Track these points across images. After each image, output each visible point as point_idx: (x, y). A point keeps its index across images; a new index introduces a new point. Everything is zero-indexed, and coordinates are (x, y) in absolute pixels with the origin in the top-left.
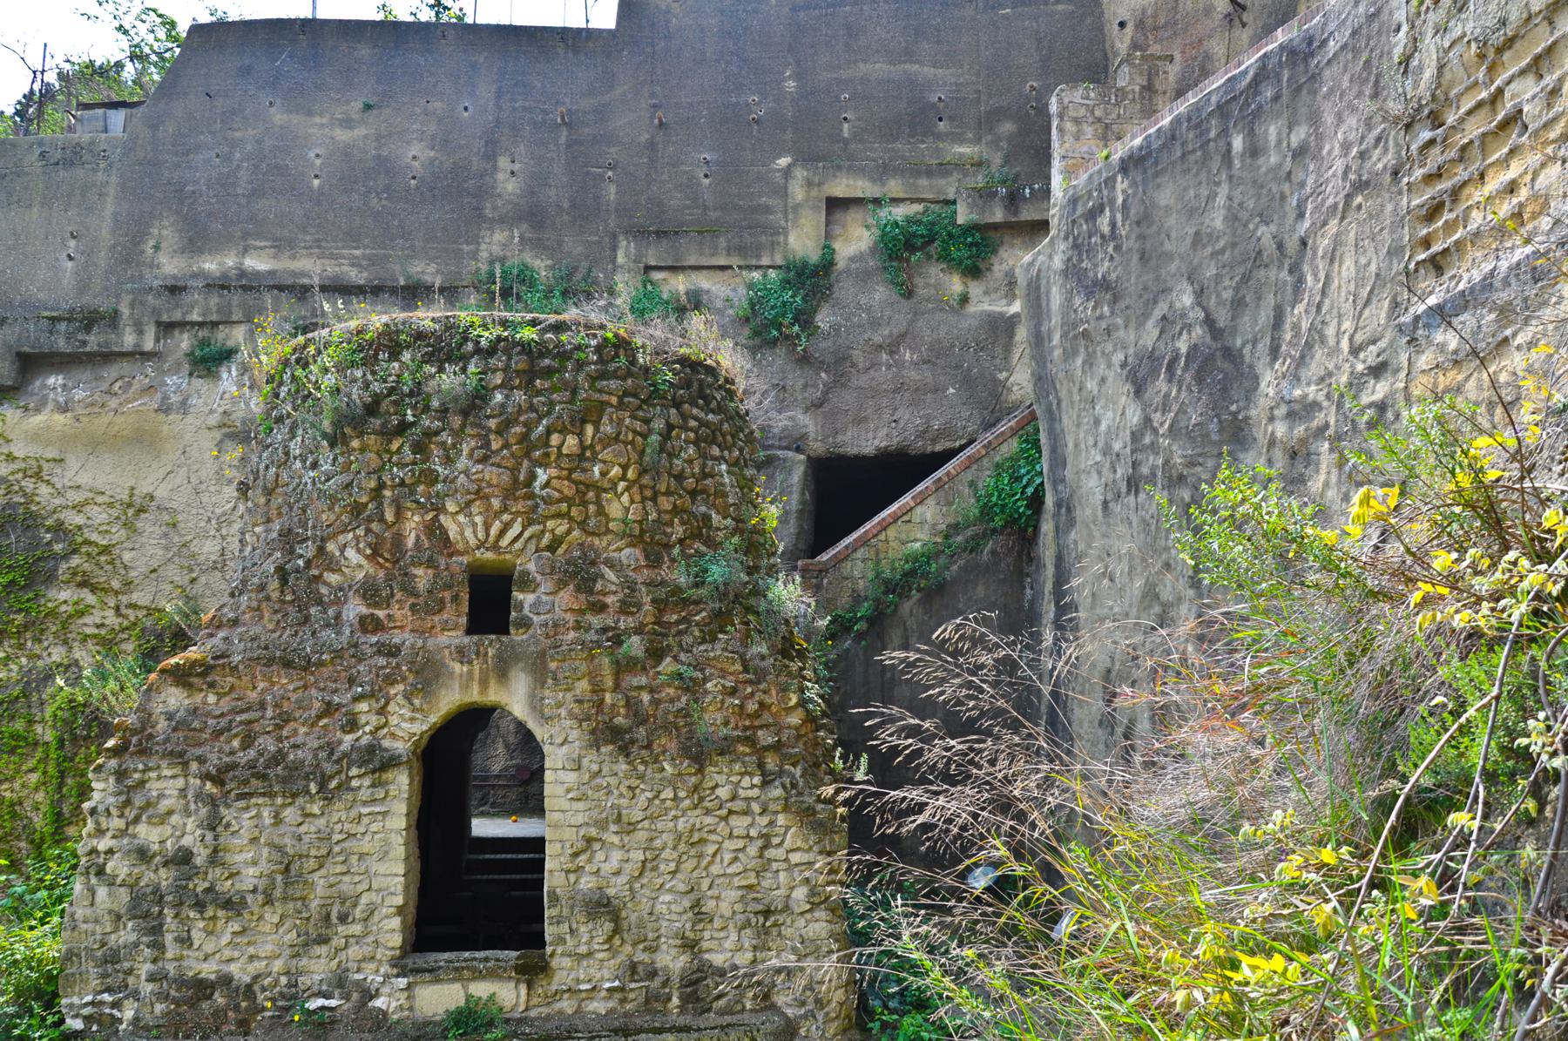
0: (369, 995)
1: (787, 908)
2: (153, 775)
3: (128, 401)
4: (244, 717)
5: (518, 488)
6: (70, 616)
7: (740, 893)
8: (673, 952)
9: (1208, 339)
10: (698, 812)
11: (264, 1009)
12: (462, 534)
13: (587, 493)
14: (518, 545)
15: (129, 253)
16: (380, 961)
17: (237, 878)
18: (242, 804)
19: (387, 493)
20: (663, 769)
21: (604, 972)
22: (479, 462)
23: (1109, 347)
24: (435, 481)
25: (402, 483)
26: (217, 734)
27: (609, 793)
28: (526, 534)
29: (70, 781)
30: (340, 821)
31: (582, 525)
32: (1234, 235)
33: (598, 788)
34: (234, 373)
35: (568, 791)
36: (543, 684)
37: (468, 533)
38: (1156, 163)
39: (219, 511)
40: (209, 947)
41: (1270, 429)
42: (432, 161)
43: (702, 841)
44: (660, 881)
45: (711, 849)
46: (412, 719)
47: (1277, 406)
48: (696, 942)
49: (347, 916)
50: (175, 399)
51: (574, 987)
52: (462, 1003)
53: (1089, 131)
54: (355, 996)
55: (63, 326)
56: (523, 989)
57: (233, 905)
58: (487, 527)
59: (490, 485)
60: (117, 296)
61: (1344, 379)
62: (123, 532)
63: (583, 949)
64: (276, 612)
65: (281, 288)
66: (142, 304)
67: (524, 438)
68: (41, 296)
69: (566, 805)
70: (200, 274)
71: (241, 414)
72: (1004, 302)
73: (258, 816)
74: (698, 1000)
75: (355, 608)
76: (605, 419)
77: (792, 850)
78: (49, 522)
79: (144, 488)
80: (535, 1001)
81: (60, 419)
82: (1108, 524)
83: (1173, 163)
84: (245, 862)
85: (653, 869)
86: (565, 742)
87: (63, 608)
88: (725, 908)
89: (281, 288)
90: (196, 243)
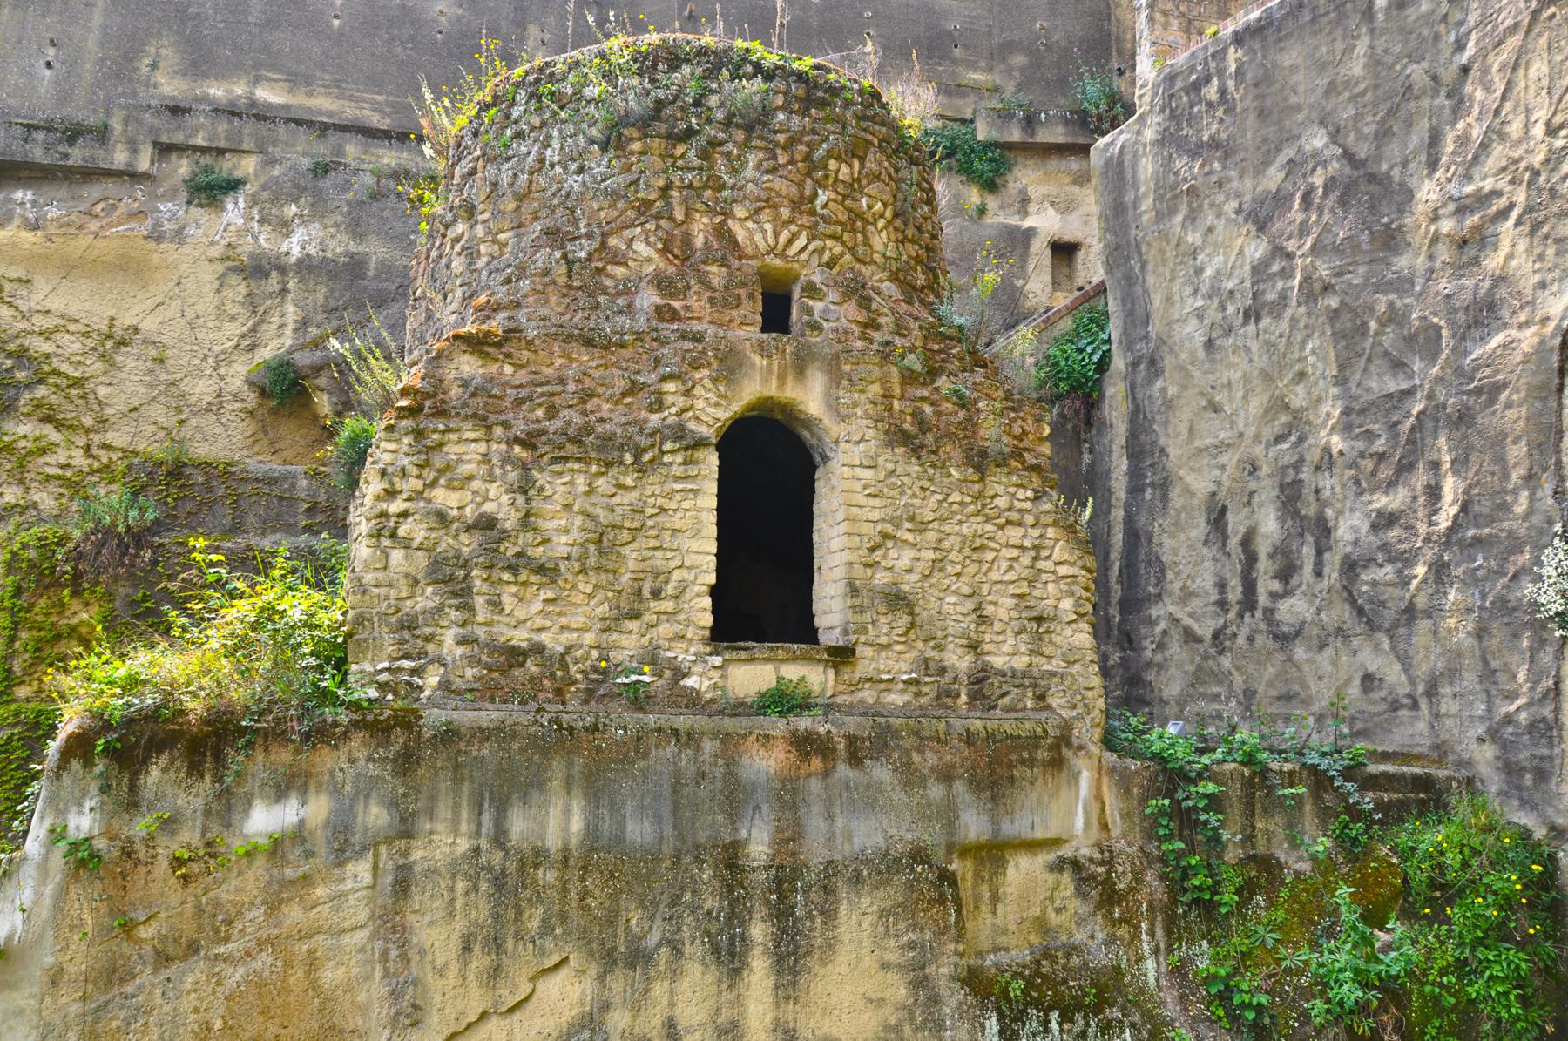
0: (680, 674)
2: (454, 437)
3: (111, 225)
4: (545, 389)
5: (802, 203)
6: (30, 453)
7: (1014, 601)
8: (959, 651)
9: (1347, 171)
10: (979, 519)
11: (575, 682)
12: (751, 239)
13: (857, 221)
14: (804, 256)
15: (121, 67)
17: (548, 545)
18: (556, 468)
19: (675, 193)
20: (950, 475)
21: (900, 665)
22: (767, 172)
23: (1221, 198)
24: (723, 187)
25: (690, 186)
26: (519, 402)
27: (903, 493)
28: (811, 247)
29: (24, 635)
30: (653, 495)
31: (852, 250)
32: (1377, 77)
33: (893, 487)
34: (241, 204)
35: (865, 487)
36: (838, 384)
37: (758, 238)
38: (1279, 30)
39: (217, 349)
40: (521, 613)
41: (1433, 228)
42: (459, 19)
43: (983, 548)
44: (947, 581)
45: (990, 556)
46: (717, 405)
47: (1444, 205)
49: (660, 591)
50: (167, 226)
51: (876, 677)
52: (774, 684)
53: (1175, 24)
54: (668, 674)
55: (40, 136)
57: (547, 571)
58: (776, 235)
59: (779, 196)
60: (107, 112)
61: (1541, 157)
62: (100, 366)
63: (884, 640)
64: (565, 296)
65: (299, 122)
66: (139, 121)
67: (808, 157)
68: (11, 101)
69: (863, 500)
70: (205, 99)
71: (248, 248)
72: (1017, 217)
73: (571, 483)
74: (984, 697)
75: (648, 299)
76: (870, 157)
77: (1060, 563)
78: (10, 347)
79: (127, 319)
80: (841, 688)
81: (28, 236)
82: (1213, 361)
83: (1301, 28)
84: (558, 530)
85: (941, 570)
86: (862, 440)
87: (23, 443)
88: (1002, 613)
89: (299, 122)
90: (199, 64)
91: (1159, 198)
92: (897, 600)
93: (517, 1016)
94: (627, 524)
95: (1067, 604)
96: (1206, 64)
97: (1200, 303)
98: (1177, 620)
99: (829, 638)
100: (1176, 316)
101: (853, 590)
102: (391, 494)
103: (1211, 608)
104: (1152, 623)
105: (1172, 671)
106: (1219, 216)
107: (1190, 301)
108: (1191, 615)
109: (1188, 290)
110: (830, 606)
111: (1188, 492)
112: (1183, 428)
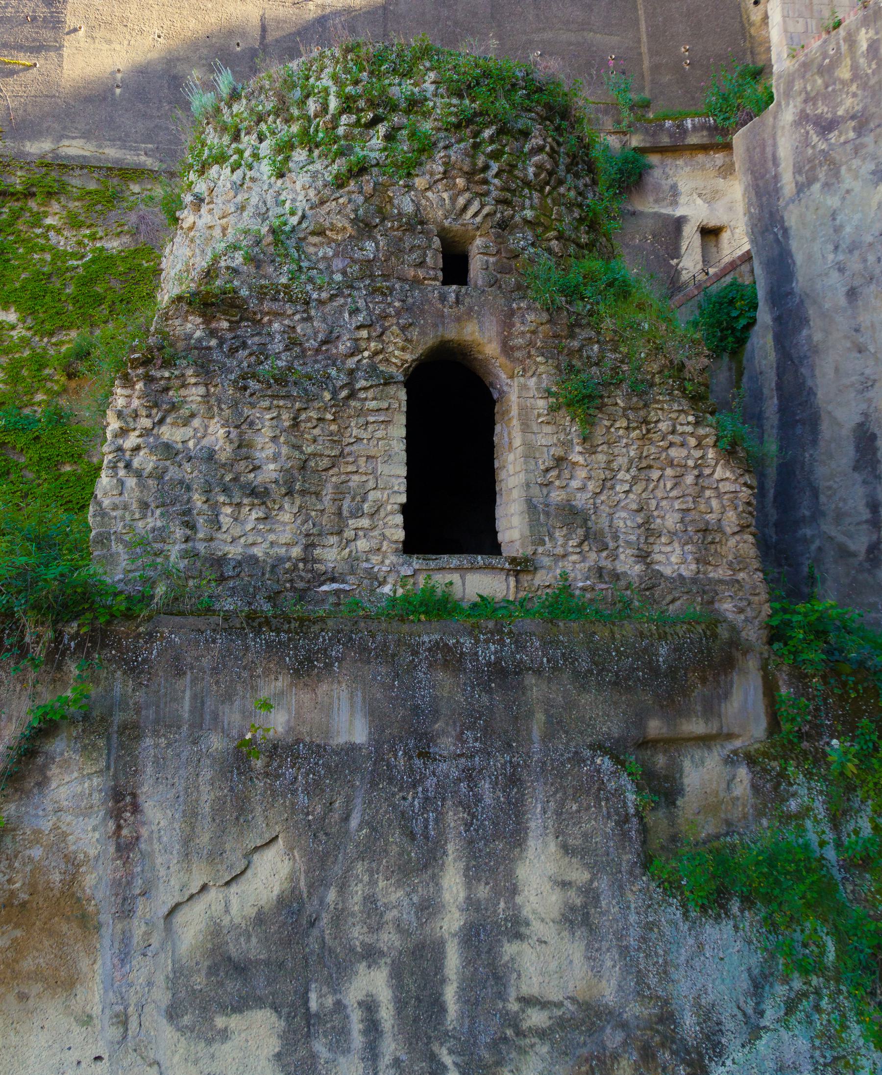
1: (720, 529)
17: (257, 472)
40: (236, 531)
46: (403, 349)
48: (649, 554)
57: (259, 494)
63: (559, 551)
73: (277, 417)
92: (573, 516)
93: (234, 888)
94: (327, 452)
95: (731, 516)
101: (531, 506)
102: (123, 432)
108: (844, 533)
109: (831, 247)
110: (512, 525)
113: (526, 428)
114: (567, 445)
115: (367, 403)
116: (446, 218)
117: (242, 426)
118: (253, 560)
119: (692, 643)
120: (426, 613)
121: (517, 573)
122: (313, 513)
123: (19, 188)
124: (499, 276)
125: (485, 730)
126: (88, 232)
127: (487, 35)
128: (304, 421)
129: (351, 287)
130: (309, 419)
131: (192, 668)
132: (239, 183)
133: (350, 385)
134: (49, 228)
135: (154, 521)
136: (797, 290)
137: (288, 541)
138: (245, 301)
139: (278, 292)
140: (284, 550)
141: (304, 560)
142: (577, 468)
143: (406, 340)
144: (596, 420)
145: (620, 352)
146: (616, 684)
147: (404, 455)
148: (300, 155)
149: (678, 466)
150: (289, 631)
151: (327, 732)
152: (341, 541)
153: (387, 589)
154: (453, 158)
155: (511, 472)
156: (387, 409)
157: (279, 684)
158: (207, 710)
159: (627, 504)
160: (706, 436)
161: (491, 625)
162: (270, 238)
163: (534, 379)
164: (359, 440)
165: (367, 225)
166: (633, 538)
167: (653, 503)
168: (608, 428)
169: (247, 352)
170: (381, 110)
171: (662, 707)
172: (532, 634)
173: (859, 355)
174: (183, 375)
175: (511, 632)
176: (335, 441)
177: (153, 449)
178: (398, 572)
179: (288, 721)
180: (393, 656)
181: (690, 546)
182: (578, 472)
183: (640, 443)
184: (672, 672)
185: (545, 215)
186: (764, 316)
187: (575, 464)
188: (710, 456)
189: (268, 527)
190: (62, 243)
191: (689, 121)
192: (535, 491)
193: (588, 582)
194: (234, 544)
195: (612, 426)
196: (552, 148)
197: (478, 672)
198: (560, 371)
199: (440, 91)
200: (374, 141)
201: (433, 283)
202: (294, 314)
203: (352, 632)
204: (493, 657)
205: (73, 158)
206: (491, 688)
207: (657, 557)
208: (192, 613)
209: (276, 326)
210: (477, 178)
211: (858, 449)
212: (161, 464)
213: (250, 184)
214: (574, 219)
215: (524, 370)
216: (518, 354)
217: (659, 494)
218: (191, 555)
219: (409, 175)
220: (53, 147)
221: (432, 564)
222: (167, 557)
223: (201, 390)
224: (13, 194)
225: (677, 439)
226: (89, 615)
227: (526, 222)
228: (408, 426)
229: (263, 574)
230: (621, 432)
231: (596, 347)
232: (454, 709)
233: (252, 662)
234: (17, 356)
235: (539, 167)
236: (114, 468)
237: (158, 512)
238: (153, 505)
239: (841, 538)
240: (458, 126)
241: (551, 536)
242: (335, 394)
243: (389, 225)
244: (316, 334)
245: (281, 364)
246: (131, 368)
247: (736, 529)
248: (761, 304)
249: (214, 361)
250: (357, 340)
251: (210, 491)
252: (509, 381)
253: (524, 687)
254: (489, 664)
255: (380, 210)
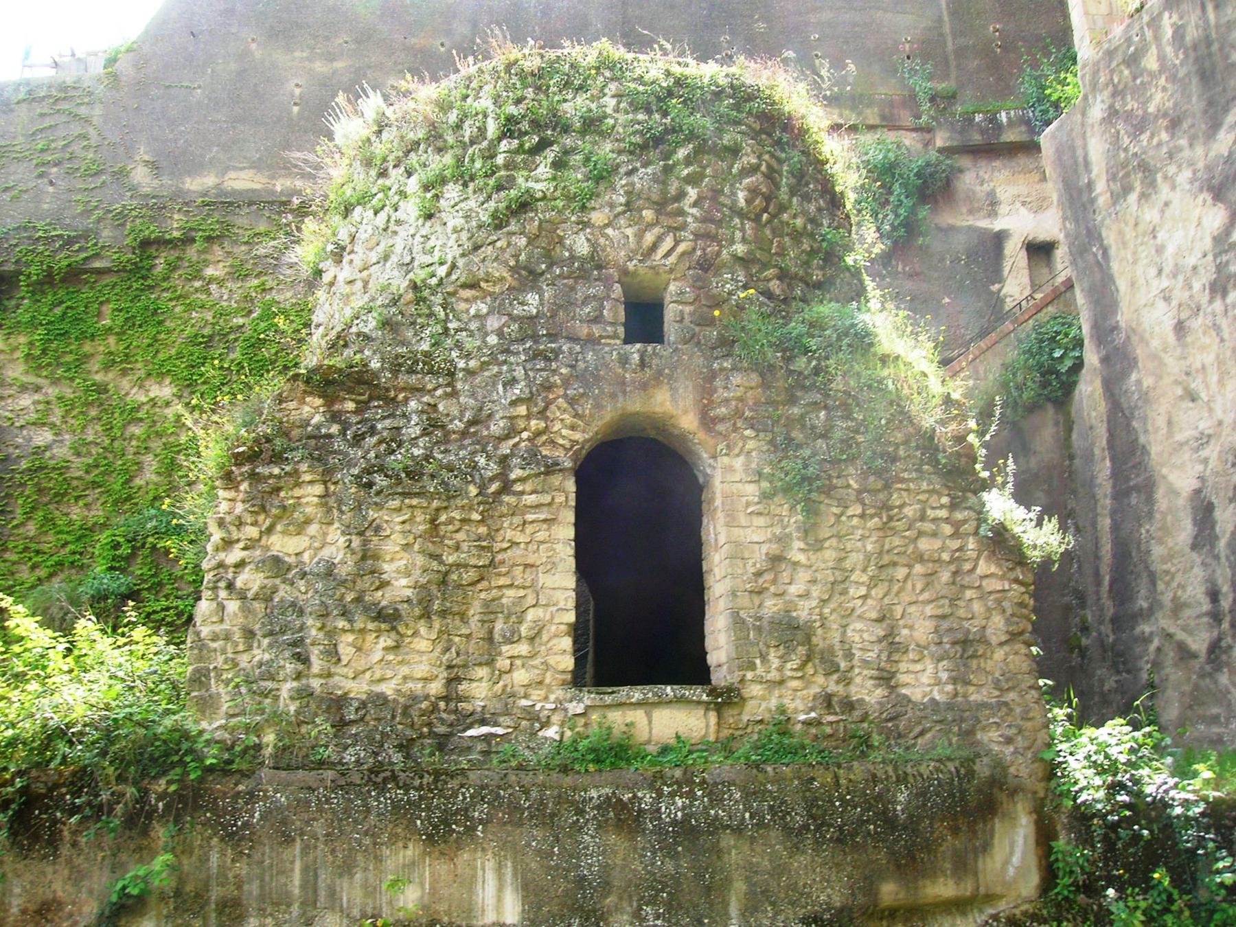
1: (984, 640)
16: (549, 686)
23: (1172, 169)
40: (361, 664)
46: (573, 428)
48: (893, 675)
56: (713, 717)
57: (387, 618)
63: (774, 675)
82: (1184, 346)
91: (1112, 178)
94: (473, 561)
95: (998, 621)
96: (1143, 34)
97: (1165, 283)
98: (1170, 636)
99: (720, 677)
100: (1143, 302)
101: (738, 622)
102: (228, 544)
103: (1205, 619)
104: (1147, 640)
105: (1169, 692)
106: (1173, 188)
107: (1155, 283)
109: (1153, 271)
111: (1173, 492)
112: (1161, 422)
113: (731, 522)
114: (783, 540)
115: (525, 497)
116: (631, 260)
117: (365, 535)
118: (380, 700)
119: (940, 785)
120: (598, 761)
121: (719, 708)
122: (457, 639)
123: (176, 234)
124: (697, 329)
125: (669, 905)
126: (256, 282)
127: (752, 16)
128: (445, 524)
129: (507, 351)
130: (451, 521)
131: (302, 834)
132: (382, 226)
133: (502, 476)
134: (211, 280)
135: (260, 654)
136: (1122, 324)
137: (425, 675)
138: (375, 375)
139: (416, 362)
140: (420, 686)
141: (446, 699)
142: (799, 569)
143: (576, 415)
144: (822, 507)
145: (854, 419)
146: (839, 840)
147: (571, 563)
148: (452, 192)
149: (928, 561)
150: (420, 788)
151: (470, 910)
152: (493, 674)
153: (552, 732)
154: (638, 186)
155: (718, 578)
156: (550, 504)
157: (409, 852)
158: (322, 885)
159: (864, 612)
160: (965, 521)
161: (678, 773)
162: (410, 296)
163: (742, 459)
164: (514, 544)
165: (531, 272)
166: (871, 656)
167: (898, 611)
168: (839, 516)
169: (375, 439)
170: (549, 132)
171: (899, 866)
172: (732, 783)
173: (1191, 405)
174: (296, 471)
175: (704, 781)
176: (483, 548)
177: (260, 565)
178: (566, 710)
179: (422, 897)
180: (553, 815)
181: (945, 662)
182: (800, 575)
183: (881, 534)
184: (912, 824)
185: (761, 249)
186: (1091, 357)
187: (796, 564)
188: (971, 546)
189: (400, 658)
190: (225, 297)
191: (1003, 114)
192: (744, 600)
193: (813, 715)
194: (357, 681)
195: (842, 514)
196: (769, 166)
197: (660, 834)
198: (775, 446)
199: (622, 105)
200: (541, 169)
201: (612, 342)
202: (435, 389)
203: (499, 787)
204: (679, 814)
205: (241, 193)
206: (677, 853)
207: (903, 678)
208: (303, 767)
209: (413, 404)
210: (669, 208)
211: (1195, 522)
212: (269, 582)
213: (396, 228)
214: (803, 251)
215: (728, 447)
216: (721, 427)
217: (906, 597)
218: (304, 694)
219: (583, 208)
220: (217, 181)
221: (608, 699)
222: (277, 698)
223: (318, 489)
224: (170, 242)
225: (928, 526)
226: (178, 770)
227: (736, 258)
228: (577, 525)
229: (393, 717)
230: (855, 521)
231: (822, 414)
232: (630, 880)
233: (375, 826)
234: (171, 439)
235: (753, 192)
236: (215, 588)
237: (266, 641)
238: (259, 633)
239: (1181, 636)
240: (644, 147)
241: (764, 658)
242: (482, 488)
243: (558, 272)
244: (462, 413)
245: (416, 452)
246: (236, 465)
247: (1004, 638)
248: (1086, 342)
249: (335, 452)
250: (512, 418)
251: (328, 615)
252: (711, 461)
253: (720, 851)
254: (674, 823)
255: (548, 256)
